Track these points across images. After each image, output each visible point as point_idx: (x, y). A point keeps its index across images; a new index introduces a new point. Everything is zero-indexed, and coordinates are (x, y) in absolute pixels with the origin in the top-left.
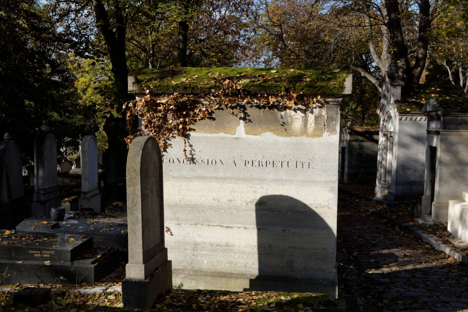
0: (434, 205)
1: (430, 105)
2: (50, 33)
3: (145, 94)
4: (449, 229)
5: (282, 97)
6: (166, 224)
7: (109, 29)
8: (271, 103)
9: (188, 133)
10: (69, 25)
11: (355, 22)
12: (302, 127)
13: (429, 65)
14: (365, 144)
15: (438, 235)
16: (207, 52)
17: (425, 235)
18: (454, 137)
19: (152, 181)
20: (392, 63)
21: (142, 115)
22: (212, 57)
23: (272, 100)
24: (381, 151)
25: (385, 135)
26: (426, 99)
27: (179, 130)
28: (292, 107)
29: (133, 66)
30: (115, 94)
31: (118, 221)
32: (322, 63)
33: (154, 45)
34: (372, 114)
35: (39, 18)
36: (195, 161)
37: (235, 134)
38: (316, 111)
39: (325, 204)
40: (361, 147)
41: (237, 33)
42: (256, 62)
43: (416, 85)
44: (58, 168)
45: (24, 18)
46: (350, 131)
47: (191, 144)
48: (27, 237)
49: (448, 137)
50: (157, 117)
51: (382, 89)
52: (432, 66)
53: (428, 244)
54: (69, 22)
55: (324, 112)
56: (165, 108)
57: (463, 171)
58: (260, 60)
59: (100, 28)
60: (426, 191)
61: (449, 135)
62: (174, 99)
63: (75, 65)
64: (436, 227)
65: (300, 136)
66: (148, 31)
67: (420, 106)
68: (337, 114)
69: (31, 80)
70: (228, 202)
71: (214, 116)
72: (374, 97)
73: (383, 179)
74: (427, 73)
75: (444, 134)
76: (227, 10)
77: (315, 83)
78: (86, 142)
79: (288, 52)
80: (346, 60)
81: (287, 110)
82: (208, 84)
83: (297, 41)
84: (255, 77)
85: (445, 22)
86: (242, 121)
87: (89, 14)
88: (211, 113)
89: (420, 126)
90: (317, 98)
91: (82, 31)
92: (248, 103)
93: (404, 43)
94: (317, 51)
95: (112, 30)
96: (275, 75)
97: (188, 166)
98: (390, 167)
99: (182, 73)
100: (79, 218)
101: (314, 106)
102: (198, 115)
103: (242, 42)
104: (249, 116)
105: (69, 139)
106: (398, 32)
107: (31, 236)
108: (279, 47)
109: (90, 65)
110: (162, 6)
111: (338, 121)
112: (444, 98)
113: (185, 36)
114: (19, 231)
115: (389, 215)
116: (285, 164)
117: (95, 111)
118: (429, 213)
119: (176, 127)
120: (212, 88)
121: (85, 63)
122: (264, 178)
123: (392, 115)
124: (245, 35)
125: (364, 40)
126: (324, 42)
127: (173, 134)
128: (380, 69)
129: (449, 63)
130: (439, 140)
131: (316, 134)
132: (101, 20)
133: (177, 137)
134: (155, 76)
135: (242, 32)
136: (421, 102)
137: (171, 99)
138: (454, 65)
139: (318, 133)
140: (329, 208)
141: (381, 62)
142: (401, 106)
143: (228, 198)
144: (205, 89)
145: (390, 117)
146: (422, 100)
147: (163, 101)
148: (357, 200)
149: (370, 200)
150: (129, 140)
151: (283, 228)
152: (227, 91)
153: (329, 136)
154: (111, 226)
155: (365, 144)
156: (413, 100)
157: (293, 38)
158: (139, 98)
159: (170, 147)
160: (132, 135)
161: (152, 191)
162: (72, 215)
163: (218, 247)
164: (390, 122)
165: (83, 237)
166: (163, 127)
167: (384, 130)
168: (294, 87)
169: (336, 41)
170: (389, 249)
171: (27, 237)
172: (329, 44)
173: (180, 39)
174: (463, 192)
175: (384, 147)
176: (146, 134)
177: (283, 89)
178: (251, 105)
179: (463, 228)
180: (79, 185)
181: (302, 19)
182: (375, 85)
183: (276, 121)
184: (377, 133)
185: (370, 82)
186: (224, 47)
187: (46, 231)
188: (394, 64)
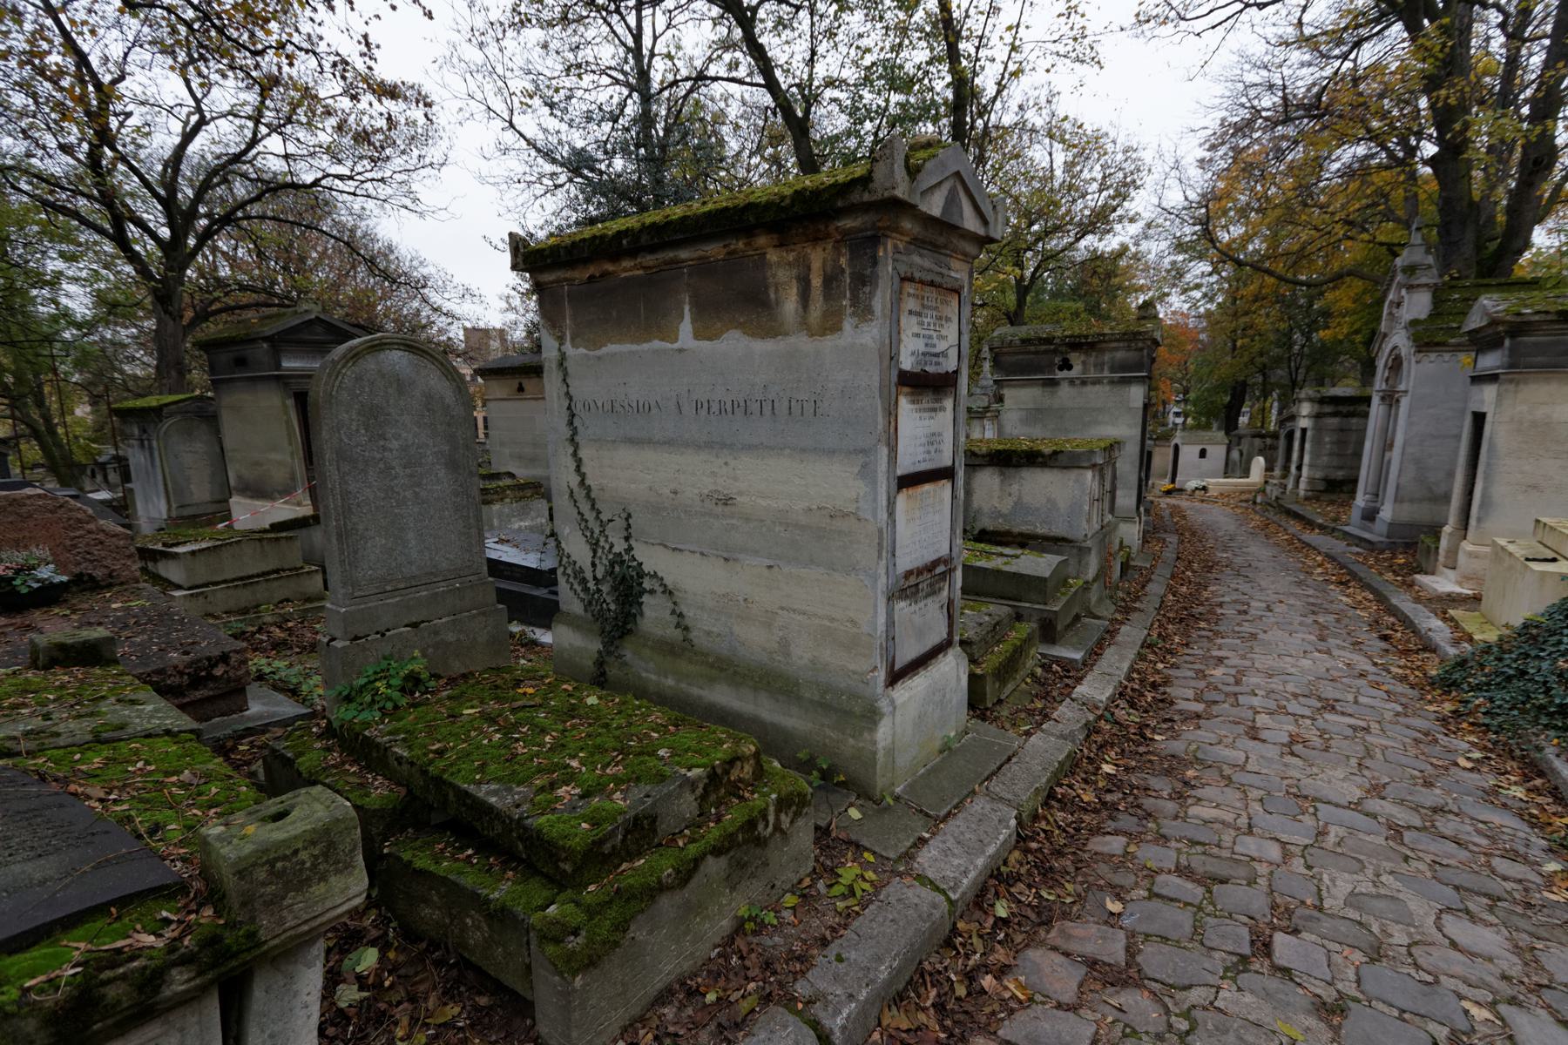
116: (767, 409)
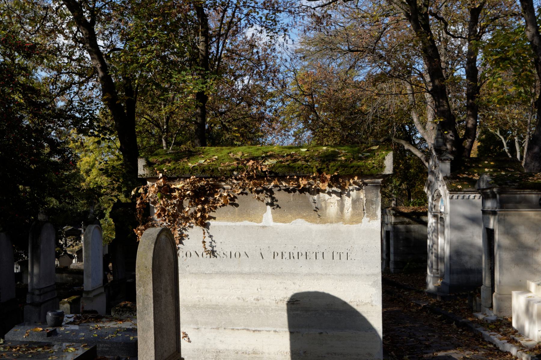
0: (496, 297)
1: (483, 181)
2: (49, 109)
3: (158, 179)
4: (514, 325)
6: (182, 329)
8: (302, 186)
9: (207, 221)
10: (72, 99)
11: (394, 90)
12: (337, 212)
13: (481, 135)
14: (412, 226)
15: (501, 333)
16: (229, 126)
17: (487, 333)
18: (513, 217)
19: (166, 279)
20: (438, 135)
21: (154, 203)
22: (235, 131)
23: (303, 182)
25: (435, 216)
26: (478, 174)
27: (196, 219)
28: (325, 190)
29: (145, 143)
30: (124, 176)
31: (127, 325)
32: (360, 136)
33: (168, 119)
36: (216, 254)
38: (354, 194)
39: (367, 301)
40: (408, 231)
41: (262, 104)
43: (467, 158)
44: (57, 262)
45: (20, 93)
46: (394, 212)
47: (211, 234)
48: (18, 348)
49: (506, 217)
50: (171, 204)
51: (429, 164)
52: (484, 136)
53: (491, 343)
54: (72, 96)
55: (362, 195)
56: (180, 194)
57: (526, 256)
58: (290, 133)
59: (107, 102)
60: (485, 280)
61: (507, 215)
62: (191, 183)
63: (79, 144)
64: (499, 323)
67: (473, 182)
68: (377, 196)
69: (27, 161)
70: (255, 301)
71: (237, 201)
72: (420, 172)
73: (434, 267)
74: (479, 144)
75: (502, 215)
76: (250, 78)
77: (351, 162)
78: (89, 232)
79: (321, 123)
80: (387, 131)
81: (320, 193)
82: (229, 166)
83: (331, 112)
84: (283, 157)
85: (495, 88)
86: (269, 207)
88: (233, 199)
89: (474, 205)
90: (353, 179)
92: (276, 186)
95: (120, 104)
97: (208, 260)
98: (443, 253)
99: (200, 154)
100: (81, 322)
101: (351, 188)
102: (219, 200)
103: (269, 114)
104: (277, 201)
106: (443, 100)
107: (23, 346)
108: (310, 119)
109: (95, 142)
110: (177, 77)
111: (378, 205)
112: (499, 173)
113: (203, 109)
114: (9, 341)
115: (443, 309)
116: (320, 256)
118: (490, 306)
119: (194, 215)
122: (295, 272)
123: (442, 193)
124: (272, 106)
125: (405, 109)
126: (362, 112)
127: (190, 224)
128: (425, 140)
130: (496, 221)
131: (354, 220)
132: (107, 93)
133: (195, 227)
134: (169, 158)
135: (268, 103)
136: (474, 178)
137: (188, 184)
138: (509, 134)
139: (356, 219)
140: (372, 306)
141: (427, 133)
142: (451, 183)
143: (255, 297)
144: (226, 171)
145: (439, 196)
146: (475, 176)
147: (179, 186)
148: (405, 293)
149: (422, 292)
150: (139, 232)
151: (320, 331)
152: (251, 173)
153: (369, 221)
154: (118, 332)
155: (412, 226)
156: (465, 176)
157: (326, 109)
158: (151, 183)
159: (186, 239)
160: (143, 225)
161: (166, 291)
162: (72, 320)
163: (243, 355)
164: (440, 202)
165: (85, 346)
166: (178, 216)
168: (328, 167)
169: (375, 111)
170: (445, 350)
171: (18, 348)
172: (366, 115)
173: (198, 113)
174: (528, 281)
176: (159, 224)
177: (315, 169)
178: (278, 188)
179: (530, 323)
180: (81, 282)
181: (335, 87)
182: (420, 159)
183: (308, 206)
184: (426, 214)
185: (416, 156)
186: (248, 119)
187: (41, 340)
188: (440, 136)
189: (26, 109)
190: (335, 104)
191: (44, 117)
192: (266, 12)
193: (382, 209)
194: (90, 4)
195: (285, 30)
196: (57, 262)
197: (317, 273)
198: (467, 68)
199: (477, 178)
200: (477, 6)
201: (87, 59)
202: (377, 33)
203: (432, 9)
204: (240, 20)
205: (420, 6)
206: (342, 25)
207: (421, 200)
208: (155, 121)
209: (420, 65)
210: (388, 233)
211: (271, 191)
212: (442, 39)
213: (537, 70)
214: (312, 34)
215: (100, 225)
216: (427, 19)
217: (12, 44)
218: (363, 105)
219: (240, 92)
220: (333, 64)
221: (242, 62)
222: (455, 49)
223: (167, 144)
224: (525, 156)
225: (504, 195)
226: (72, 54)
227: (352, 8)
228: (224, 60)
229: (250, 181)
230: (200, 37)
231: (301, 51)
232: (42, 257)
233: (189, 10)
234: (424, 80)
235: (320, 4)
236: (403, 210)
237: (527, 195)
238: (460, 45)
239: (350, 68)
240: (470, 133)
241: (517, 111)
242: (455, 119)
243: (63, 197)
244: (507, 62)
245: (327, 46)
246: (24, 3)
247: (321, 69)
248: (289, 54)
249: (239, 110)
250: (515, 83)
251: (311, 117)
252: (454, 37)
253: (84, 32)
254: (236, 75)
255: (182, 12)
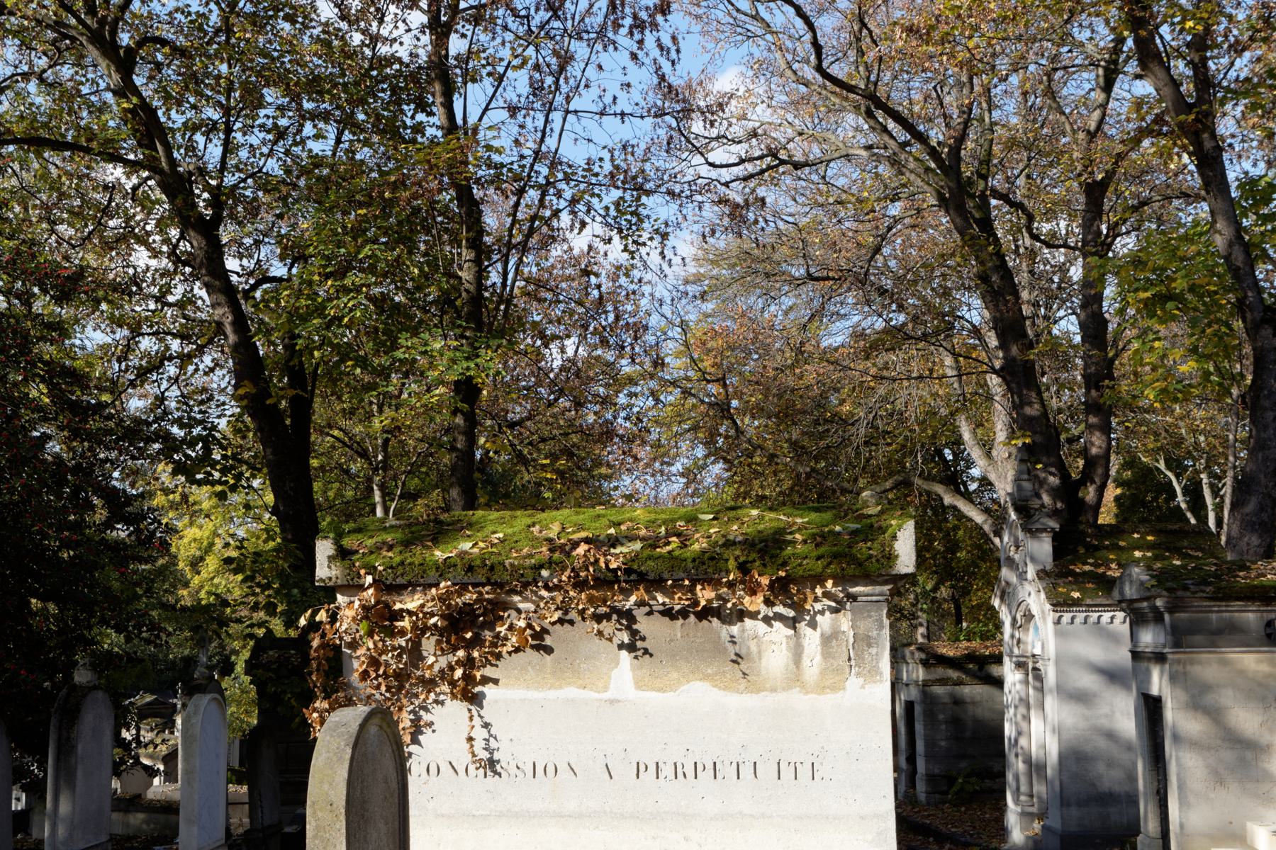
1: (1131, 582)
2: (110, 417)
3: (362, 588)
5: (731, 585)
7: (268, 402)
8: (703, 603)
9: (478, 689)
10: (163, 393)
18: (1209, 666)
19: (380, 832)
21: (354, 645)
23: (705, 595)
24: (1012, 711)
25: (1020, 665)
26: (1119, 565)
27: (453, 684)
28: (759, 612)
29: (331, 494)
30: (281, 575)
33: (386, 441)
34: (979, 606)
35: (78, 378)
36: (498, 768)
37: (606, 689)
38: (825, 621)
40: (958, 702)
41: (606, 401)
42: (662, 472)
43: (1090, 526)
45: (43, 380)
46: (923, 656)
47: (487, 719)
49: (1188, 668)
50: (394, 649)
51: (1002, 541)
58: (674, 469)
59: (244, 403)
61: (1192, 663)
62: (441, 599)
63: (177, 497)
65: (784, 689)
66: (371, 403)
67: (1107, 584)
68: (881, 627)
71: (548, 641)
74: (1119, 491)
75: (1179, 662)
78: (195, 713)
79: (745, 445)
81: (746, 619)
82: (531, 556)
83: (769, 418)
87: (217, 365)
88: (539, 635)
89: (1113, 638)
90: (823, 586)
91: (196, 409)
92: (641, 603)
93: (1048, 419)
94: (822, 444)
95: (275, 405)
96: (711, 526)
97: (479, 782)
98: (1042, 752)
99: (463, 528)
101: (818, 606)
102: (506, 639)
104: (643, 639)
105: (149, 698)
108: (720, 435)
112: (1166, 563)
116: (747, 771)
117: (223, 622)
120: (541, 566)
121: (202, 495)
123: (1035, 610)
125: (944, 412)
127: (437, 695)
128: (991, 484)
129: (1176, 465)
130: (1166, 677)
131: (827, 683)
132: (246, 382)
133: (448, 702)
135: (622, 399)
137: (433, 600)
139: (830, 683)
141: (995, 465)
142: (1055, 586)
145: (1029, 616)
146: (1110, 569)
150: (315, 715)
153: (863, 687)
156: (1087, 568)
158: (346, 599)
159: (428, 731)
160: (324, 698)
164: (1031, 630)
166: (409, 676)
167: (1016, 651)
169: (871, 416)
172: (853, 424)
175: (1021, 699)
176: (363, 697)
177: (732, 564)
178: (647, 609)
183: (718, 649)
184: (998, 660)
185: (970, 520)
186: (575, 438)
189: (55, 419)
190: (780, 399)
191: (96, 439)
192: (616, 194)
193: (893, 649)
194: (211, 178)
195: (665, 236)
196: (115, 784)
197: (740, 813)
198: (1083, 316)
199: (1117, 574)
200: (1100, 177)
201: (200, 303)
202: (871, 239)
203: (997, 182)
204: (556, 213)
205: (969, 178)
206: (790, 219)
207: (986, 625)
208: (358, 443)
209: (975, 311)
210: (909, 706)
211: (629, 616)
212: (1022, 250)
213: (1244, 322)
214: (722, 242)
215: (221, 692)
216: (985, 206)
217: (26, 266)
218: (842, 402)
219: (557, 376)
220: (773, 308)
221: (561, 306)
222: (1054, 273)
223: (383, 497)
224: (1226, 520)
225: (1183, 615)
226: (167, 290)
227: (813, 183)
228: (521, 303)
229: (580, 592)
230: (464, 252)
231: (698, 279)
232: (80, 774)
233: (440, 191)
234: (985, 345)
235: (741, 174)
236: (944, 651)
237: (1237, 614)
238: (1064, 264)
239: (813, 316)
240: (1095, 466)
241: (1202, 413)
242: (1058, 435)
243: (134, 627)
244: (1170, 305)
245: (759, 268)
246: (60, 177)
247: (746, 321)
248: (670, 287)
249: (554, 416)
250: (1194, 350)
251: (722, 430)
252: (1049, 246)
253: (195, 243)
254: (546, 336)
255: (423, 195)
